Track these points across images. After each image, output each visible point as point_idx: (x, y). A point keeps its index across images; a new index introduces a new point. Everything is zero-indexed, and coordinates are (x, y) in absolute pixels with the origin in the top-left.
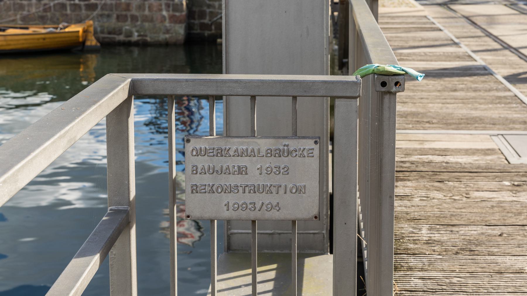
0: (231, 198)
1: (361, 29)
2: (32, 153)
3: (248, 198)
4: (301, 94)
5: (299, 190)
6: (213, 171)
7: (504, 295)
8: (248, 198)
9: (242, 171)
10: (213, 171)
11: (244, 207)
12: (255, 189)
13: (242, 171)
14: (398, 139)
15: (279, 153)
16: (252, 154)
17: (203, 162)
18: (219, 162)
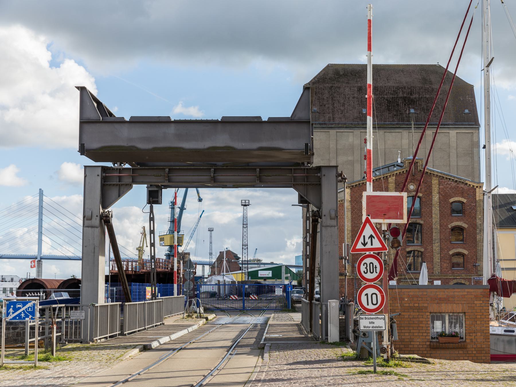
0: (75, 317)
1: (79, 67)
2: (427, 270)
3: (77, 317)
4: (420, 382)
5: (83, 316)
6: (73, 314)
7: (138, 383)
8: (77, 317)
9: (77, 314)
10: (73, 314)
11: (77, 318)
12: (78, 316)
13: (77, 314)
14: (36, 248)
15: (81, 312)
16: (78, 312)
17: (72, 313)
18: (74, 313)
